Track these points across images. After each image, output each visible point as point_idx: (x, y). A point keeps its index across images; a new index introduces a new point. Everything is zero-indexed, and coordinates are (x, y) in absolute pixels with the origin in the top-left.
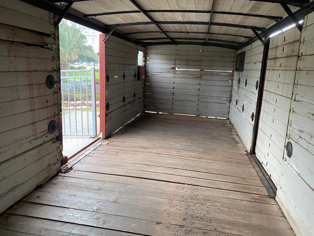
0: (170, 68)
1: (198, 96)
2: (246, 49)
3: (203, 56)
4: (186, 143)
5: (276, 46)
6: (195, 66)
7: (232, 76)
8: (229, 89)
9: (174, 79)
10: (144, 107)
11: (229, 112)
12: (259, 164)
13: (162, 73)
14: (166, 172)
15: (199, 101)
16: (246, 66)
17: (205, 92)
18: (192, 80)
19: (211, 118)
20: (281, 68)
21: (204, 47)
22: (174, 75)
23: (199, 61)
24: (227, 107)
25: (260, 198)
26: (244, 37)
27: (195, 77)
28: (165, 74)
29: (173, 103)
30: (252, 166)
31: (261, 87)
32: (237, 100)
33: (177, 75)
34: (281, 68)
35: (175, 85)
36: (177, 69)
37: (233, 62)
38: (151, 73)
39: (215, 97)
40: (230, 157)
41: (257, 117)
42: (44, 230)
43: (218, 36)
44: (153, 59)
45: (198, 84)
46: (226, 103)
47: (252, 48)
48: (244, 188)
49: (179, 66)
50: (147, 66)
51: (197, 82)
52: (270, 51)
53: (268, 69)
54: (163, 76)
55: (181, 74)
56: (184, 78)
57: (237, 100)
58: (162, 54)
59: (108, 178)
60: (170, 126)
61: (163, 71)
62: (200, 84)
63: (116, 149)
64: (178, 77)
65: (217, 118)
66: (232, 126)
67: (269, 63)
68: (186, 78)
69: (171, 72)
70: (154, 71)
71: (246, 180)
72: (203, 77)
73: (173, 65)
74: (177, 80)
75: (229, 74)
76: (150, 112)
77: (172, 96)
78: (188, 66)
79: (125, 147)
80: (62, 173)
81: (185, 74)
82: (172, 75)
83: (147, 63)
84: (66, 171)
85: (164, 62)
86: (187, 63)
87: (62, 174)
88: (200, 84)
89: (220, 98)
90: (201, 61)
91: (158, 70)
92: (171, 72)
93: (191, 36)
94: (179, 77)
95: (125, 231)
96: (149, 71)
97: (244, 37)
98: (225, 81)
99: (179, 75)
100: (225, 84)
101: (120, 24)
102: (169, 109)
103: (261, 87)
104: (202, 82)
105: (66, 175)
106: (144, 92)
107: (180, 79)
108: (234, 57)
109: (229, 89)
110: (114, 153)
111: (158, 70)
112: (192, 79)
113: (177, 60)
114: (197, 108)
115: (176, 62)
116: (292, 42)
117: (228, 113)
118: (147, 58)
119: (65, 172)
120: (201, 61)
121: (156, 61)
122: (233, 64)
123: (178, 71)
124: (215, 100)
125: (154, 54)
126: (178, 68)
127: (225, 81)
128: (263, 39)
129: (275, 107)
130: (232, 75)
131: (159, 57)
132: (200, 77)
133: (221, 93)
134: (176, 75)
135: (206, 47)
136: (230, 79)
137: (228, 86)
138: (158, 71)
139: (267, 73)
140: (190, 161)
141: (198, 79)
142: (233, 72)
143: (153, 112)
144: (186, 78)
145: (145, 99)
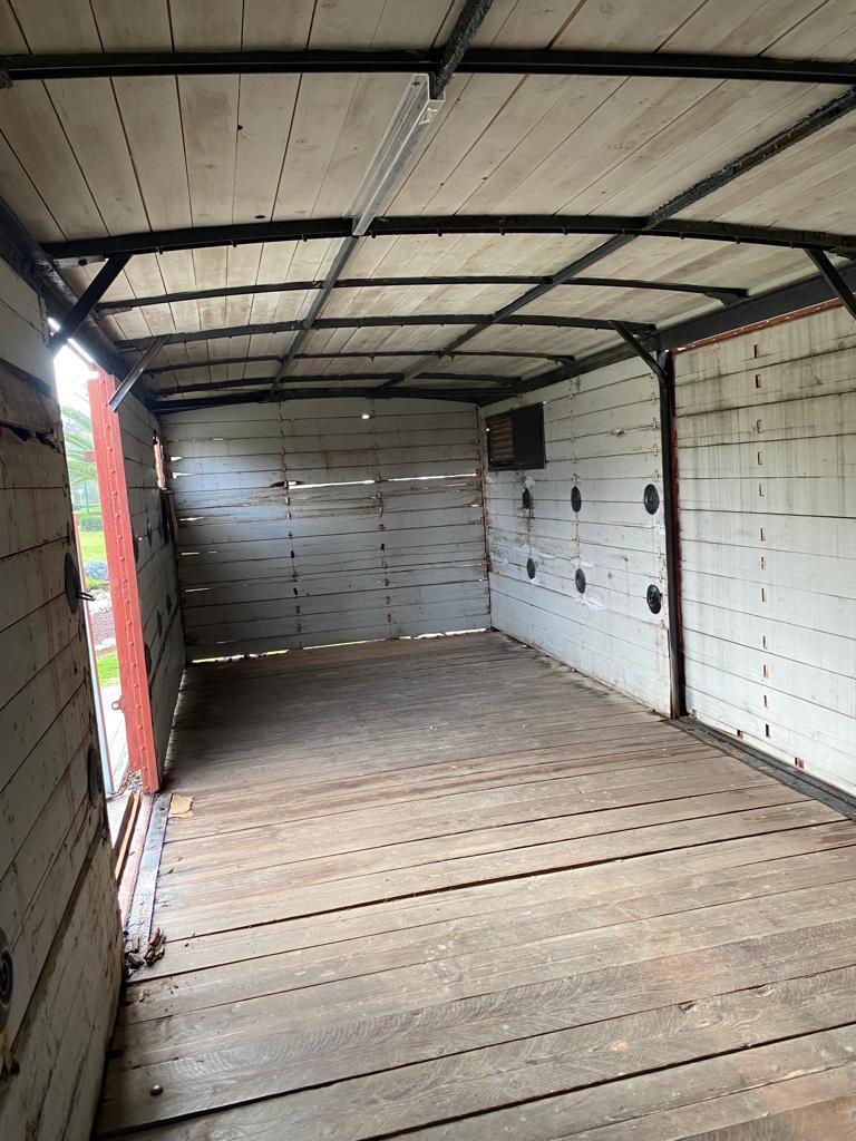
0: (268, 484)
1: (383, 570)
2: (544, 396)
3: (377, 433)
4: (464, 733)
5: (716, 374)
6: (358, 468)
7: (480, 488)
8: (477, 531)
9: (287, 522)
10: (186, 644)
11: (489, 607)
12: (730, 743)
13: (240, 505)
14: (513, 841)
15: (391, 586)
16: (551, 451)
17: (406, 551)
18: (352, 517)
19: (455, 635)
20: (762, 437)
21: (282, 407)
22: (286, 508)
23: (366, 450)
24: (481, 591)
25: (839, 833)
26: (550, 357)
27: (361, 508)
28: (249, 509)
29: (298, 607)
30: (720, 753)
31: (667, 500)
32: (530, 561)
33: (299, 507)
34: (762, 437)
35: (296, 544)
36: (292, 486)
37: (473, 443)
38: (196, 512)
39: (437, 566)
40: (636, 741)
41: (670, 599)
42: (804, 1115)
43: (313, 363)
44: (197, 461)
45: (376, 528)
46: (477, 578)
47: (582, 389)
48: (771, 818)
49: (299, 476)
50: (175, 486)
51: (372, 521)
52: (679, 393)
53: (689, 442)
54: (246, 517)
55: (312, 500)
56: (323, 513)
57: (530, 561)
58: (228, 439)
59: (340, 926)
60: (343, 690)
61: (242, 500)
62: (382, 528)
63: (250, 819)
64: (301, 514)
65: (448, 634)
66: (529, 647)
67: (683, 428)
68: (332, 515)
69: (273, 498)
70: (212, 503)
71: (749, 793)
72: (391, 504)
73: (279, 474)
74: (299, 526)
75: (469, 484)
76: (213, 660)
77: (294, 585)
78: (330, 471)
79: (272, 801)
80: (137, 966)
81: (326, 498)
82: (278, 510)
83: (175, 475)
84: (153, 955)
85: (240, 465)
86: (329, 457)
87: (144, 974)
88: (382, 528)
89: (453, 564)
90: (374, 449)
91: (223, 497)
92: (273, 498)
93: (235, 372)
94: (306, 514)
95: (621, 1074)
96: (185, 506)
97: (550, 357)
98: (462, 507)
99: (304, 508)
100: (463, 516)
101: (171, 335)
102: (289, 631)
103: (667, 500)
104: (388, 520)
105: (162, 968)
106: (179, 588)
107: (311, 520)
108: (474, 429)
109: (477, 531)
110: (258, 834)
111: (223, 497)
112: (354, 514)
113: (287, 455)
114: (387, 611)
115: (286, 462)
116: (806, 358)
117: (486, 611)
118: (173, 459)
119: (152, 961)
120: (374, 449)
121: (208, 465)
122: (473, 451)
123: (295, 492)
124: (440, 576)
125: (198, 440)
126: (298, 483)
127: (462, 507)
128: (654, 354)
129: (764, 553)
130: (479, 486)
131: (220, 449)
132: (377, 503)
133: (454, 548)
134: (292, 508)
135: (380, 404)
136: (473, 498)
137: (473, 523)
138: (224, 502)
139: (685, 460)
140: (544, 786)
141: (371, 510)
142: (480, 472)
143: (213, 660)
144: (331, 513)
145: (186, 612)
